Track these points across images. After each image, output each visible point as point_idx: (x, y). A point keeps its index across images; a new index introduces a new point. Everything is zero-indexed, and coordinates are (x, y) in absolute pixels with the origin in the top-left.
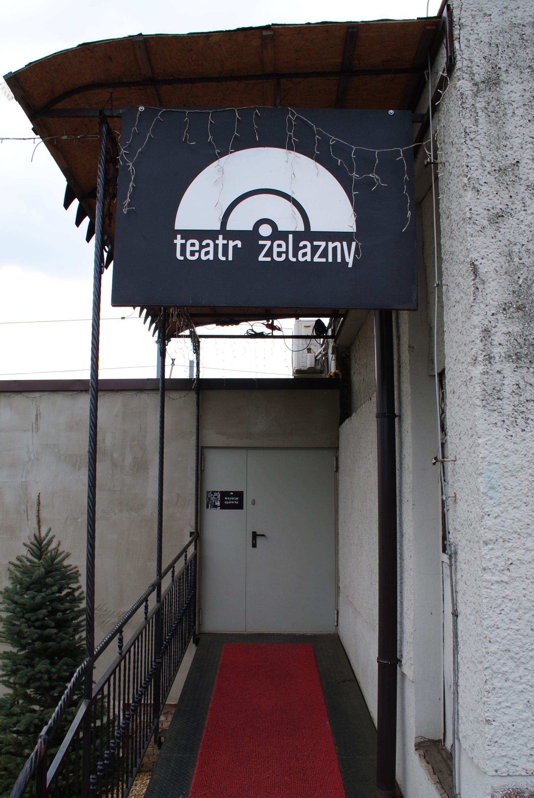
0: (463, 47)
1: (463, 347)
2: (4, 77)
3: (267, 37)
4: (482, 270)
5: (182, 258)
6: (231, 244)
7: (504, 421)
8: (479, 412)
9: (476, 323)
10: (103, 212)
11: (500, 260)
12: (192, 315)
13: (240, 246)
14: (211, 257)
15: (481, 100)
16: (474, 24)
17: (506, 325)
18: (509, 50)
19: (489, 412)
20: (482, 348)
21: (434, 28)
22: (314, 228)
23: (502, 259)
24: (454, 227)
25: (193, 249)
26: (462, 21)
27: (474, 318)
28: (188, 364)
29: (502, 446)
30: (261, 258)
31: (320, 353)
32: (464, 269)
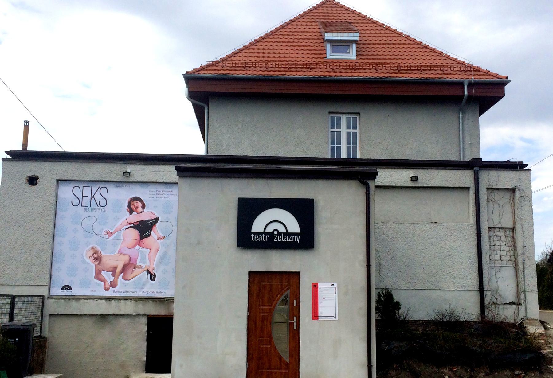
22: (289, 232)
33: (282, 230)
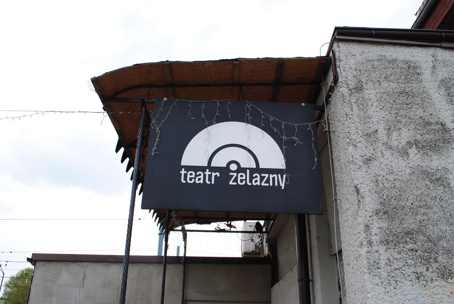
0: (342, 71)
1: (353, 236)
2: (91, 79)
3: (236, 64)
4: (362, 190)
5: (184, 182)
6: (214, 174)
7: (382, 282)
8: (366, 276)
9: (360, 222)
10: (140, 154)
11: (371, 184)
12: (184, 218)
13: (218, 175)
14: (201, 181)
15: (354, 98)
16: (347, 60)
17: (378, 223)
18: (367, 73)
19: (373, 277)
20: (365, 237)
21: (325, 61)
22: (261, 167)
23: (373, 184)
24: (342, 166)
25: (191, 176)
26: (341, 58)
27: (359, 218)
28: (176, 248)
29: (383, 298)
30: (231, 183)
31: (258, 242)
32: (351, 190)
33: (247, 162)
